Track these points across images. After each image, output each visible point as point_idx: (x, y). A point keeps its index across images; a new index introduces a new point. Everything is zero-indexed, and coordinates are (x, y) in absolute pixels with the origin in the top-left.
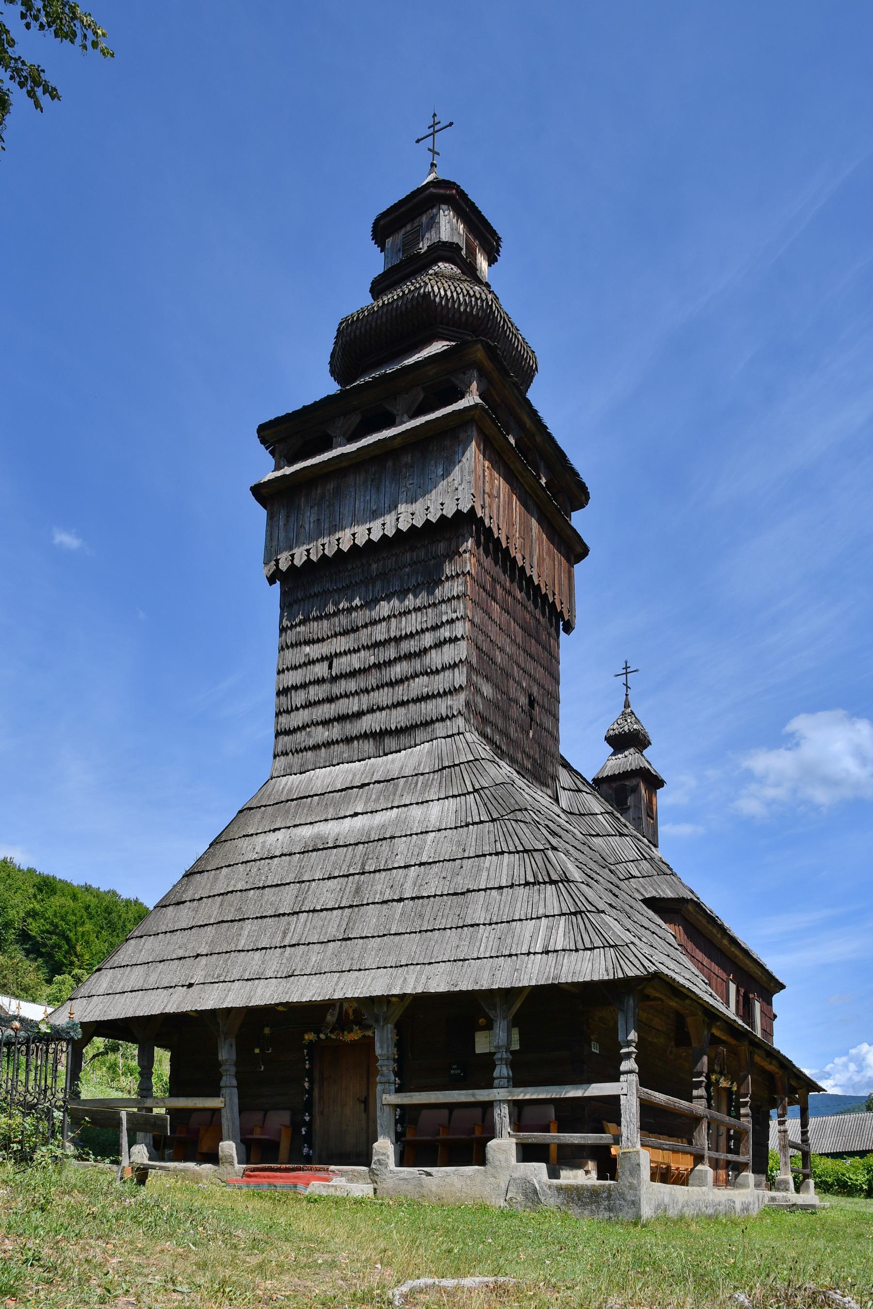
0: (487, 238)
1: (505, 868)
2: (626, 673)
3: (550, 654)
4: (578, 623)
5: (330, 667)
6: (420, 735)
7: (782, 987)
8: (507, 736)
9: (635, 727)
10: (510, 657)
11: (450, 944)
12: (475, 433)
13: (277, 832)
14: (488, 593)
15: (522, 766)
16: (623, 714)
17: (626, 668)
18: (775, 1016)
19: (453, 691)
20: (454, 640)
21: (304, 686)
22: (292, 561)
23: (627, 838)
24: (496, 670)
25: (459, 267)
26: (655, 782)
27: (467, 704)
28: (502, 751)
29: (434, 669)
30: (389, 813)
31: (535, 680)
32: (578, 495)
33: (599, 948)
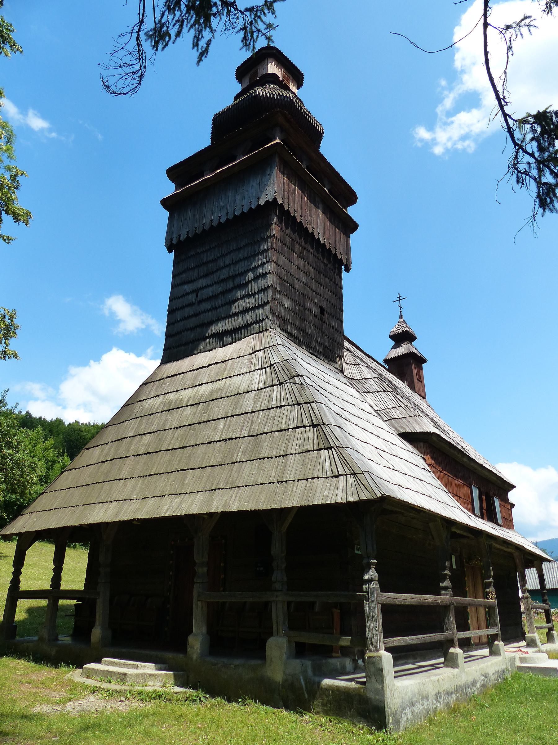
0: (298, 77)
1: (290, 416)
2: (400, 300)
3: (335, 283)
4: (353, 266)
5: (197, 296)
6: (244, 332)
7: (513, 487)
8: (304, 332)
9: (406, 329)
10: (256, 268)
11: (248, 472)
12: (277, 160)
13: (158, 397)
14: (289, 248)
15: (315, 350)
16: (399, 322)
17: (399, 297)
18: (513, 505)
19: (265, 304)
20: (264, 275)
21: (183, 308)
22: (179, 238)
23: (389, 393)
24: (295, 293)
25: (276, 85)
26: (420, 361)
27: (272, 311)
28: (300, 341)
29: (253, 292)
30: (220, 382)
31: (324, 298)
32: (350, 197)
33: (342, 475)
